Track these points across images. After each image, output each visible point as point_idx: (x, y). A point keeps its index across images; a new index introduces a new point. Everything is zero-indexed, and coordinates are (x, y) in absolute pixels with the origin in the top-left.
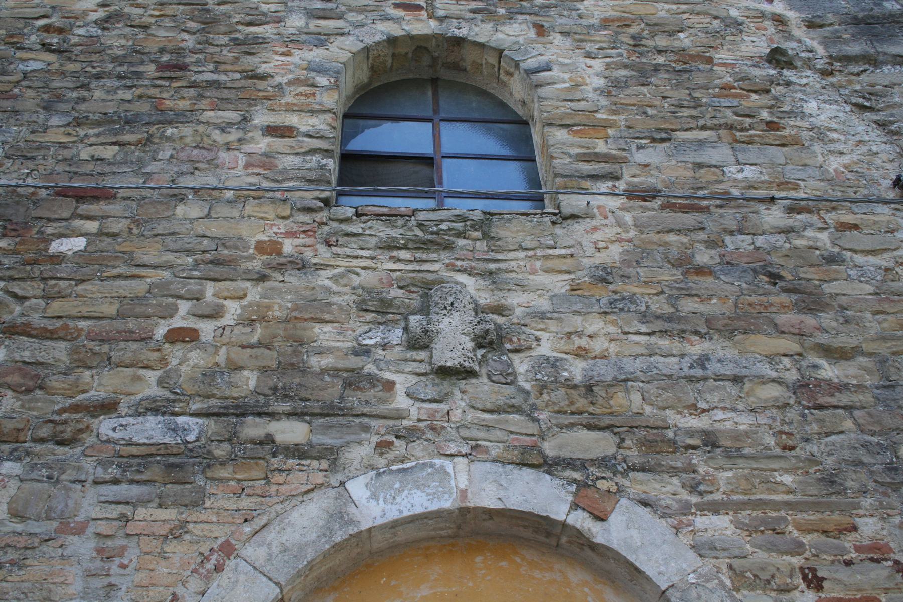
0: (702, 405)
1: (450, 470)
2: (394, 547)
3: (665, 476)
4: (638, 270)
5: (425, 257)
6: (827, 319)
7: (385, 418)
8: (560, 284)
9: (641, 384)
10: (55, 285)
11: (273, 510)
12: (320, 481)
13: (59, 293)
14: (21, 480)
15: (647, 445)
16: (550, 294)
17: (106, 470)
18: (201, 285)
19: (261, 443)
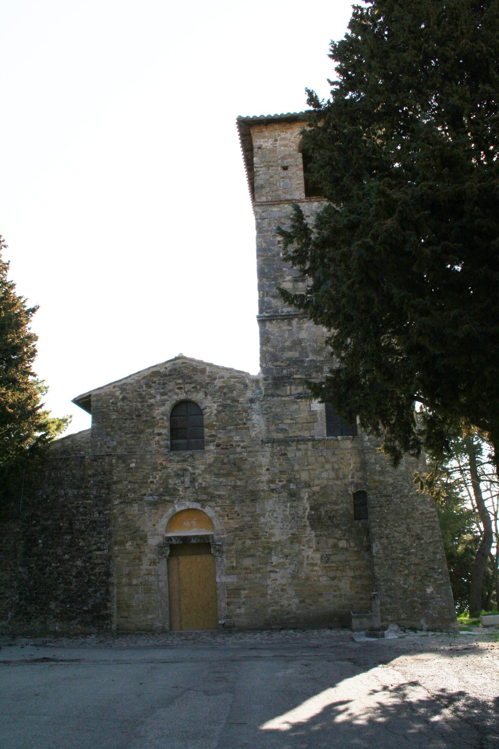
6: (241, 473)
15: (211, 497)
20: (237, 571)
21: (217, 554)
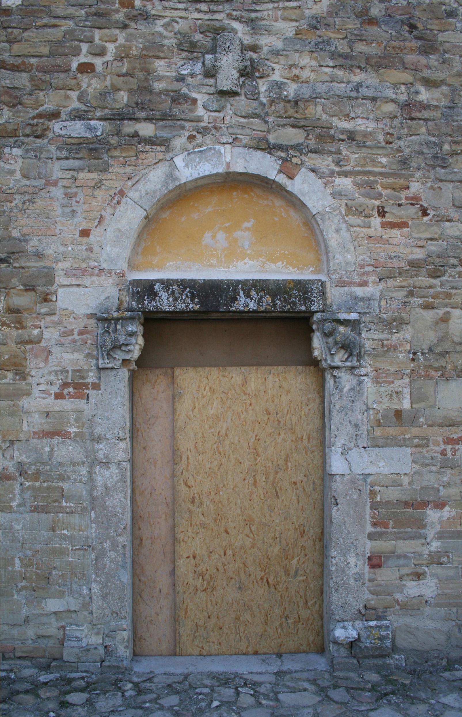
0: (352, 115)
1: (223, 152)
2: (197, 188)
3: (326, 156)
4: (336, 19)
5: (215, 9)
6: (433, 60)
7: (192, 121)
8: (290, 29)
9: (323, 100)
10: (12, 32)
11: (140, 173)
12: (161, 158)
13: (15, 38)
14: (23, 158)
15: (320, 138)
16: (284, 37)
17: (61, 152)
18: (91, 31)
19: (133, 136)
20: (416, 431)
21: (337, 362)
